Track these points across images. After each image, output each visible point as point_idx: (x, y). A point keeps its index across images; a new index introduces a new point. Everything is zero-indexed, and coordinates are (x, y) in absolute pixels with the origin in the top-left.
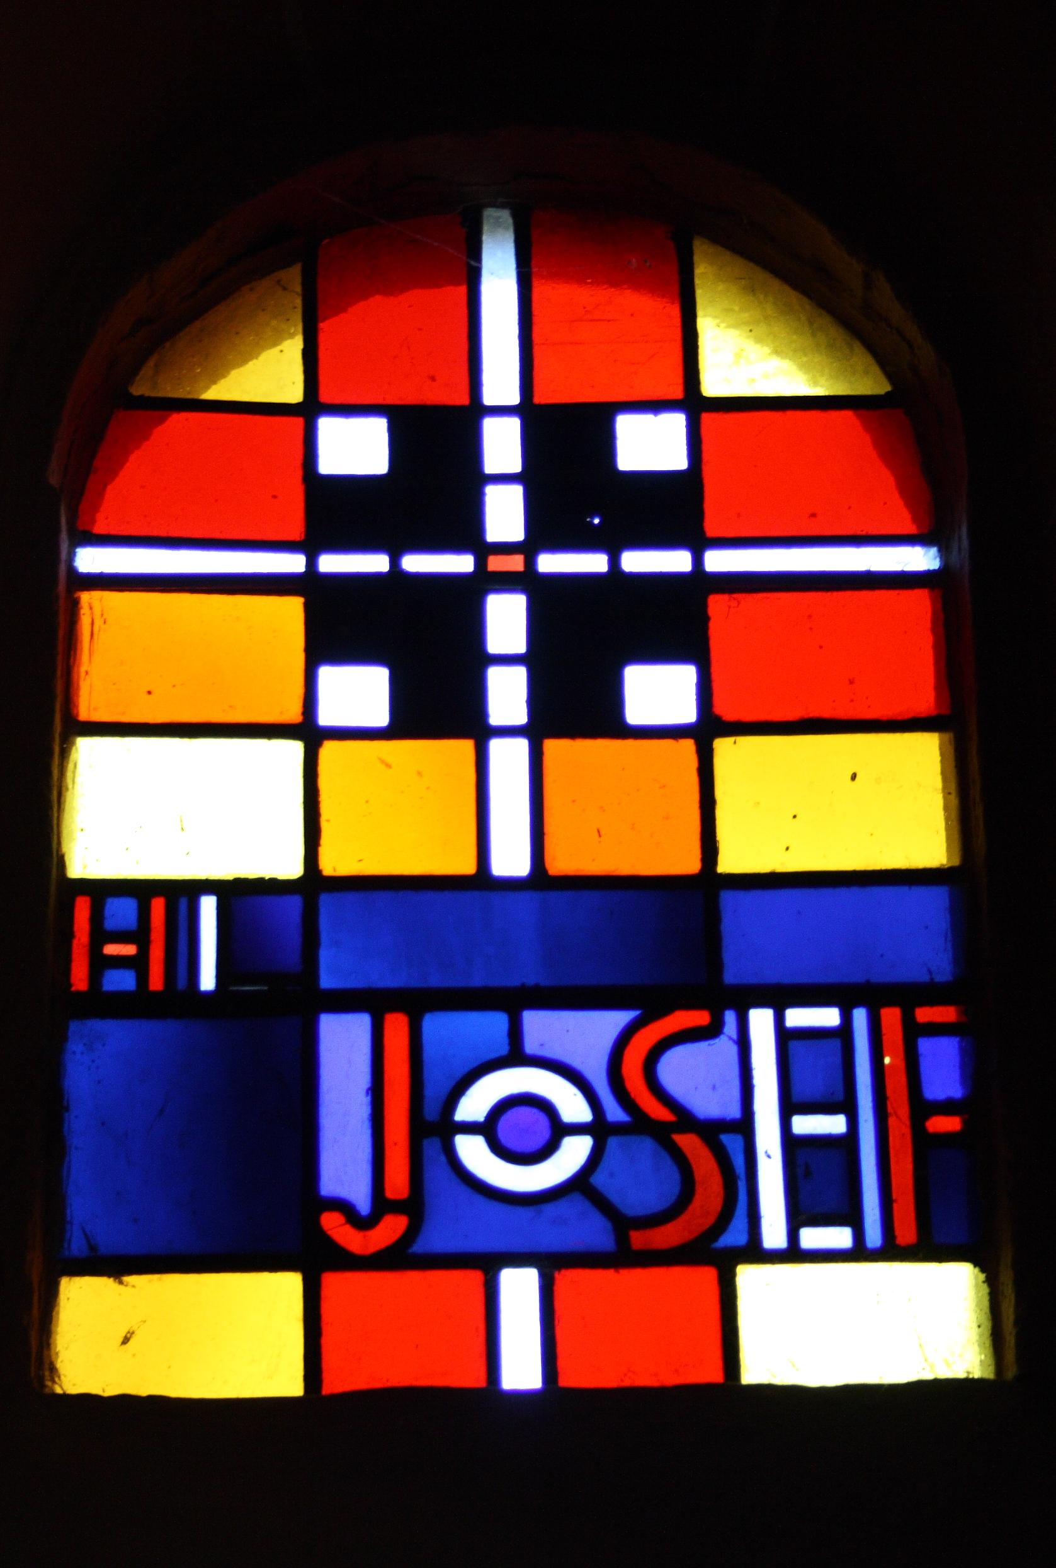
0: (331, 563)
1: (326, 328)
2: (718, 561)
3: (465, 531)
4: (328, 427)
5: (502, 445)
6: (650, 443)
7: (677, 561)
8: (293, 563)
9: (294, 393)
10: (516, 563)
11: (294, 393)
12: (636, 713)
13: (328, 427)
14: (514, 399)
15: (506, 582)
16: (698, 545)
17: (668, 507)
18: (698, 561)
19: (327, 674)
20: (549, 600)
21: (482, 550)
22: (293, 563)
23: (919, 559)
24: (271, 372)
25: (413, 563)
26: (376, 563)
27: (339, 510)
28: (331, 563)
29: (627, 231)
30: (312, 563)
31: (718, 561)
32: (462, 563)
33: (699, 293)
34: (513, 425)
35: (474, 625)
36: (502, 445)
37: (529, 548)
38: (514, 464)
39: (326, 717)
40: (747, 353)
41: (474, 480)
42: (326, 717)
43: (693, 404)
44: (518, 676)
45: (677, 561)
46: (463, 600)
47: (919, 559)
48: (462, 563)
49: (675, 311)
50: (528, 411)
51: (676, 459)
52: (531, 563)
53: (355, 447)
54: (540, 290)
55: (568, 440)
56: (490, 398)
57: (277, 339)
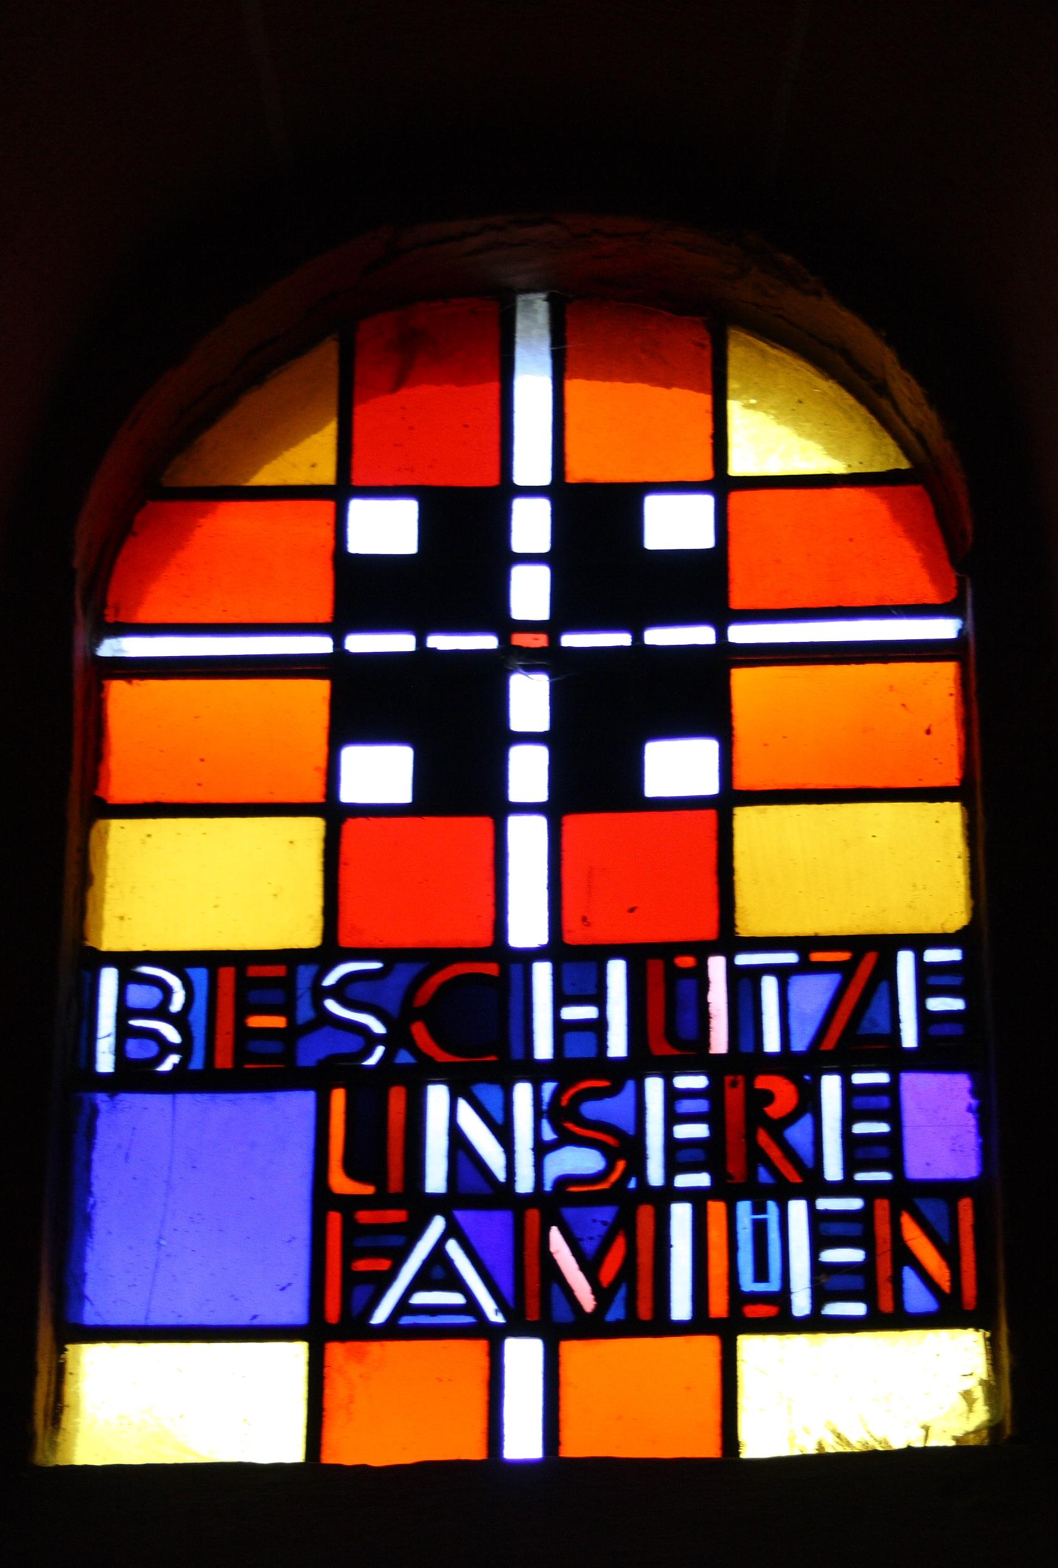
0: (358, 643)
1: (361, 414)
2: (740, 634)
3: (491, 611)
4: (359, 510)
5: (531, 526)
6: (677, 524)
7: (703, 635)
8: (322, 645)
9: (326, 474)
10: (540, 641)
11: (326, 474)
12: (655, 786)
13: (359, 510)
14: (515, 823)
15: (532, 661)
16: (721, 619)
17: (697, 584)
18: (721, 634)
19: (707, 541)
20: (572, 678)
21: (505, 626)
22: (322, 645)
23: (945, 629)
24: (312, 458)
25: (439, 642)
26: (403, 642)
27: (366, 589)
28: (358, 643)
29: (661, 318)
30: (339, 643)
31: (740, 634)
32: (488, 642)
33: (732, 371)
34: (515, 794)
35: (498, 702)
36: (531, 526)
37: (553, 627)
38: (542, 543)
39: (705, 503)
40: (777, 433)
41: (505, 560)
42: (705, 503)
43: (722, 485)
44: (520, 543)
45: (703, 635)
46: (486, 679)
47: (945, 629)
48: (488, 642)
49: (705, 401)
50: (498, 808)
51: (703, 538)
52: (554, 640)
53: (386, 527)
54: (573, 387)
55: (598, 517)
56: (520, 478)
57: (316, 428)
